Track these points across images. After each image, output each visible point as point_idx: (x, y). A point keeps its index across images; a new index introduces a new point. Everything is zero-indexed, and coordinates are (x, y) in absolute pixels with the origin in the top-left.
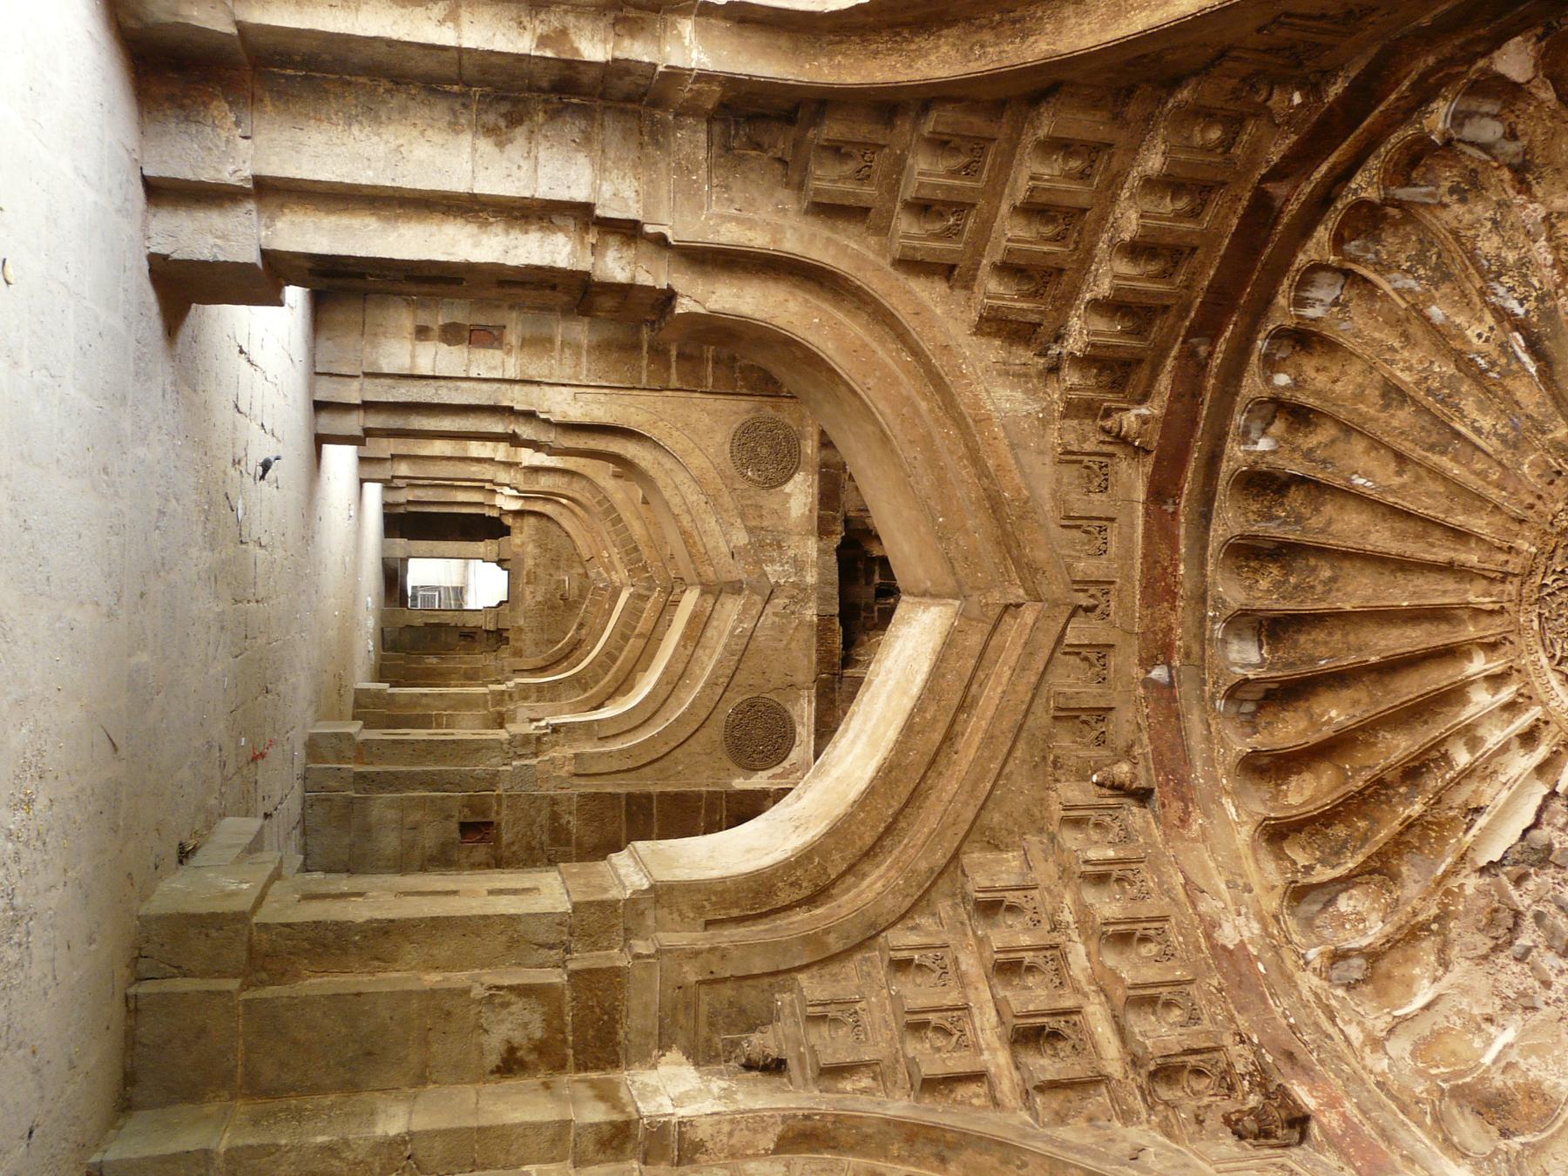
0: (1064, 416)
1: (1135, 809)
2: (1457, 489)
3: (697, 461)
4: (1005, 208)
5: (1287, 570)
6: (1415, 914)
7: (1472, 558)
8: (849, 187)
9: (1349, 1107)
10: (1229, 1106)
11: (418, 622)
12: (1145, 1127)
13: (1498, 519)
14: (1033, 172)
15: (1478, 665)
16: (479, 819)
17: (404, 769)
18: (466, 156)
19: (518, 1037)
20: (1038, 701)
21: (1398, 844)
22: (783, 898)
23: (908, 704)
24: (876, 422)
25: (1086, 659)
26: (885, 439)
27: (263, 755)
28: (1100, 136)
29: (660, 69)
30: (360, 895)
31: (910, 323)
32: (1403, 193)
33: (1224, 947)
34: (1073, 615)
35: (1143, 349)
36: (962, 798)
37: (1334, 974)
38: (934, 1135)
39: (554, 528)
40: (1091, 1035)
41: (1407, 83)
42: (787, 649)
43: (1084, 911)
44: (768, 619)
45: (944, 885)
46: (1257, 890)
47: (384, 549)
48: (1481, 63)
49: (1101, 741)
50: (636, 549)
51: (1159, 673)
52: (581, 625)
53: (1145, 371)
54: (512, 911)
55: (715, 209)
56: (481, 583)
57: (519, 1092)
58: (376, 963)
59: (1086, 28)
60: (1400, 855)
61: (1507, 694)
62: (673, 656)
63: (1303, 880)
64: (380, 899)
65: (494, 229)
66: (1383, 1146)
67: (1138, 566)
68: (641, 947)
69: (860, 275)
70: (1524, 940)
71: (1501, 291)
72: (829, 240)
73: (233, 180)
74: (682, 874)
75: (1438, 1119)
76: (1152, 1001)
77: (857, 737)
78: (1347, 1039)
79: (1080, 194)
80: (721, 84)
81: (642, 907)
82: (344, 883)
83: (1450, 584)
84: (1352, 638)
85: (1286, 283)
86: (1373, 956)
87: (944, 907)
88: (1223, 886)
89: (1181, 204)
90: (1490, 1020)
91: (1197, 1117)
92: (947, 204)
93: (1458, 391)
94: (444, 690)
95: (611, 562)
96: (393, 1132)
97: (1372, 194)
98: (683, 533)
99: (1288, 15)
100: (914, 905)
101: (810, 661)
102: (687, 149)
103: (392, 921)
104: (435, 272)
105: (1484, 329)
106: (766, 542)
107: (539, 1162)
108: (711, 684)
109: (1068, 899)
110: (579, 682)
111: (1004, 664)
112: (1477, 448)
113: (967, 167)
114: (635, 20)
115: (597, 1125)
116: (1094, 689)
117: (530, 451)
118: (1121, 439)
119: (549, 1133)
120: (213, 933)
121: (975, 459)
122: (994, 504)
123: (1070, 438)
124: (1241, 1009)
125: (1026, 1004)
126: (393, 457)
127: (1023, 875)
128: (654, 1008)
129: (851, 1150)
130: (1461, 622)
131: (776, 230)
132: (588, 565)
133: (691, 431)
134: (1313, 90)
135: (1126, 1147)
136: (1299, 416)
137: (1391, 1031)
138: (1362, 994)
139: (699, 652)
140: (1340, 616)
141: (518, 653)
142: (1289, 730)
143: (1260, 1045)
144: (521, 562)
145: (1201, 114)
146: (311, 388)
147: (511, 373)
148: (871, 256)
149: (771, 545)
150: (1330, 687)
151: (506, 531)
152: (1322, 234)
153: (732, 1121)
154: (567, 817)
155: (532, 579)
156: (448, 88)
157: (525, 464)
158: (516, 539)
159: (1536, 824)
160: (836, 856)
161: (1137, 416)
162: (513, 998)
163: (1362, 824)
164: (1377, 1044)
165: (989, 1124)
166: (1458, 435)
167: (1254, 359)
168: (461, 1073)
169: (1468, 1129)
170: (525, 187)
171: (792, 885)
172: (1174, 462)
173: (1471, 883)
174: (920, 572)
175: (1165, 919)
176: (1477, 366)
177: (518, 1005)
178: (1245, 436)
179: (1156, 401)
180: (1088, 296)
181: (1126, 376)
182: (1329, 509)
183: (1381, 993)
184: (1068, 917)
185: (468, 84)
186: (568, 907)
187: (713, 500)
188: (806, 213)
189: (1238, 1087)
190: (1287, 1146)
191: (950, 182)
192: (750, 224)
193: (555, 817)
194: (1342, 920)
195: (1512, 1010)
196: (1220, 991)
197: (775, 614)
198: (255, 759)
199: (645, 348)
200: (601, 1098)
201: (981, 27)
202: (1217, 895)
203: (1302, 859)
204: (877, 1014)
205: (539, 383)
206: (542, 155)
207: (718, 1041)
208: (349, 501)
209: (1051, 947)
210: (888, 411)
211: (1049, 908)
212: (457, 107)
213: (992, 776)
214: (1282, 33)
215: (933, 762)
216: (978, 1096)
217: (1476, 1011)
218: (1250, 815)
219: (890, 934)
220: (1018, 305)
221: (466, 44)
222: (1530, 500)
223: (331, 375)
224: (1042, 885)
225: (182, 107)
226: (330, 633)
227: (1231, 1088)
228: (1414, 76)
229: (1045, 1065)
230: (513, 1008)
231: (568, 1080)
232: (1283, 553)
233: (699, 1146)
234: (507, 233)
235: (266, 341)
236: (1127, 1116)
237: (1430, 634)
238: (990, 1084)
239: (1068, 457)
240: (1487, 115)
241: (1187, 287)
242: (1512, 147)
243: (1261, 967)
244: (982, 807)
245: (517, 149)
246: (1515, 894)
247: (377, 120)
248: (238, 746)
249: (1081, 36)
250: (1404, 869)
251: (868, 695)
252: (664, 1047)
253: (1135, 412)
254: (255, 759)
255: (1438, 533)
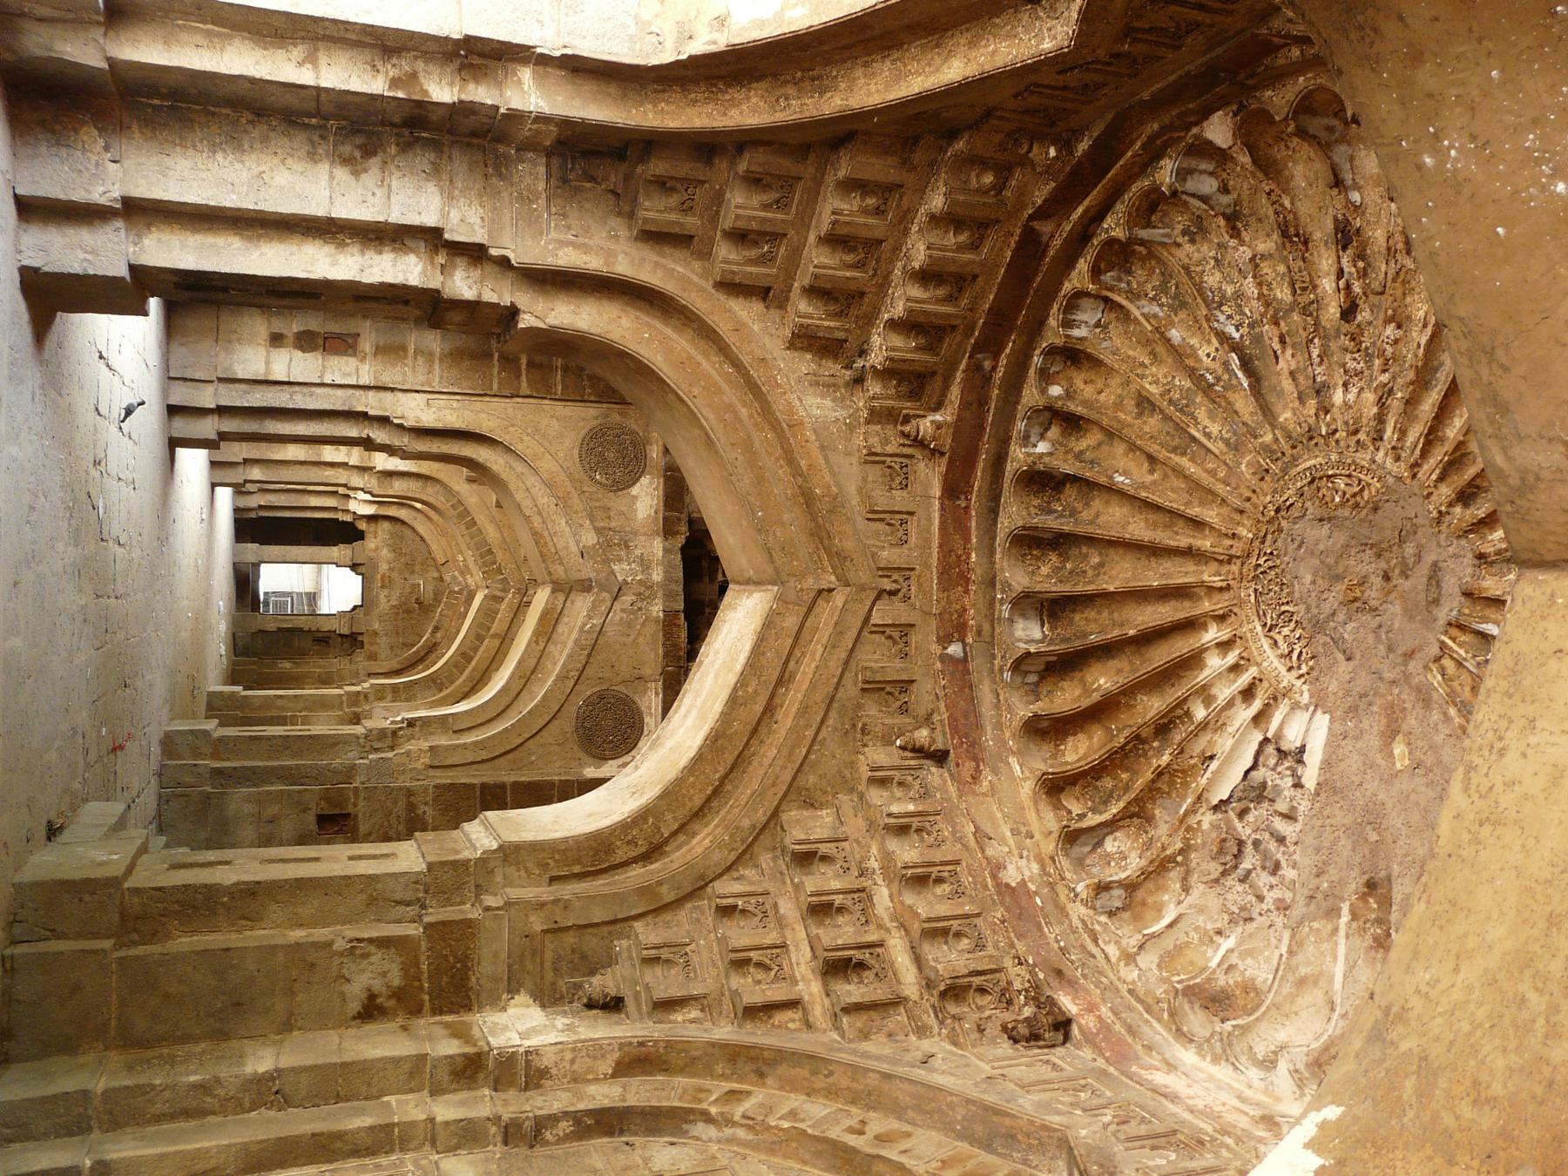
0: (868, 422)
1: (933, 769)
2: (1194, 485)
3: (547, 465)
4: (812, 238)
5: (1065, 557)
6: (1164, 848)
7: (1205, 543)
8: (673, 217)
9: (1104, 1011)
10: (1007, 1017)
11: (271, 627)
12: (937, 1039)
13: (1225, 511)
14: (834, 208)
15: (1212, 634)
16: (337, 811)
17: (261, 764)
18: (324, 183)
19: (378, 985)
20: (847, 674)
21: (1152, 791)
22: (621, 855)
23: (732, 679)
24: (702, 427)
25: (890, 637)
26: (709, 442)
27: (122, 748)
28: (891, 179)
29: (502, 110)
30: (227, 863)
31: (731, 338)
32: (1144, 234)
33: (1007, 885)
34: (878, 598)
35: (936, 364)
36: (780, 762)
37: (1098, 904)
38: (753, 1053)
39: (408, 532)
40: (892, 965)
41: (1139, 144)
42: (635, 643)
43: (887, 857)
44: (617, 615)
45: (766, 839)
46: (1037, 836)
47: (235, 553)
48: (1195, 130)
49: (904, 710)
50: (490, 552)
51: (955, 649)
52: (436, 629)
53: (937, 383)
54: (371, 872)
55: (553, 234)
56: (337, 589)
57: (379, 1034)
58: (243, 922)
59: (873, 88)
60: (1153, 800)
61: (1231, 658)
62: (525, 651)
63: (1075, 825)
64: (244, 866)
65: (350, 249)
66: (1130, 1040)
67: (935, 554)
68: (490, 901)
69: (685, 295)
70: (1246, 864)
71: (1222, 318)
72: (657, 263)
73: (103, 201)
74: (528, 836)
75: (1173, 1014)
76: (944, 932)
77: (688, 712)
78: (1107, 957)
79: (875, 226)
80: (557, 125)
81: (492, 865)
82: (211, 855)
83: (1190, 566)
84: (1116, 615)
85: (1056, 307)
86: (1131, 887)
87: (765, 860)
88: (1008, 834)
89: (962, 238)
90: (1219, 933)
91: (979, 1026)
92: (762, 234)
93: (1194, 402)
94: (299, 692)
95: (466, 566)
96: (261, 1069)
97: (1119, 233)
98: (535, 533)
99: (1037, 85)
100: (739, 858)
101: (657, 655)
102: (528, 180)
103: (258, 883)
104: (295, 287)
105: (1211, 349)
106: (614, 542)
107: (399, 1092)
108: (562, 678)
109: (874, 850)
110: (435, 682)
111: (818, 642)
112: (1209, 450)
113: (778, 202)
114: (479, 67)
115: (451, 1057)
116: (898, 663)
117: (384, 455)
118: (919, 443)
119: (407, 1066)
120: (87, 898)
121: (790, 459)
122: (807, 499)
123: (874, 440)
124: (1020, 936)
125: (835, 939)
126: (246, 461)
127: (836, 829)
128: (504, 955)
129: (681, 1071)
130: (1200, 598)
131: (610, 255)
132: (443, 569)
133: (541, 436)
134: (1066, 145)
135: (919, 1055)
136: (1073, 423)
137: (1141, 947)
138: (1121, 919)
139: (551, 647)
140: (1106, 596)
141: (373, 657)
142: (1066, 697)
143: (1035, 965)
144: (375, 567)
145: (974, 161)
146: (165, 393)
147: (365, 380)
148: (695, 278)
149: (619, 545)
150: (1099, 659)
151: (360, 536)
152: (1083, 265)
153: (574, 1050)
154: (423, 808)
155: (387, 583)
156: (307, 121)
157: (379, 468)
158: (370, 543)
159: (1254, 767)
160: (669, 816)
161: (932, 422)
162: (372, 949)
163: (1124, 776)
164: (1129, 958)
165: (802, 1042)
166: (1194, 439)
167: (1032, 372)
168: (325, 1019)
169: (1197, 1021)
170: (379, 212)
171: (628, 843)
172: (968, 463)
173: (1207, 819)
174: (744, 562)
175: (957, 862)
176: (1206, 380)
177: (377, 956)
178: (1026, 440)
179: (949, 409)
180: (886, 316)
181: (922, 387)
182: (1097, 504)
183: (1137, 918)
184: (874, 864)
185: (326, 118)
186: (421, 866)
187: (563, 502)
188: (636, 239)
189: (1015, 1001)
190: (1053, 1046)
191: (763, 214)
192: (585, 249)
193: (411, 807)
194: (1108, 858)
195: (1236, 923)
196: (1003, 922)
197: (623, 610)
198: (114, 750)
199: (496, 356)
200: (455, 1035)
201: (786, 82)
202: (1003, 842)
203: (1076, 808)
204: (705, 955)
205: (392, 390)
206: (395, 183)
207: (562, 985)
208: (201, 504)
209: (859, 891)
210: (711, 417)
211: (858, 856)
212: (316, 138)
213: (807, 742)
214: (1034, 100)
215: (755, 731)
216: (793, 1021)
217: (1209, 926)
218: (1032, 771)
219: (716, 884)
220: (826, 323)
221: (324, 85)
222: (1248, 494)
223: (185, 380)
224: (852, 837)
225: (53, 132)
226: (183, 634)
227: (1010, 1002)
228: (1144, 138)
229: (851, 991)
230: (373, 959)
231: (423, 1023)
232: (1060, 542)
233: (544, 1073)
234: (363, 254)
235: (123, 350)
236: (922, 1031)
237: (1176, 610)
238: (804, 1009)
239: (872, 458)
240: (1205, 172)
241: (971, 310)
242: (1225, 200)
243: (1038, 900)
244: (799, 770)
245: (371, 178)
246: (1239, 825)
247: (239, 148)
248: (99, 736)
249: (869, 94)
250: (1157, 812)
251: (698, 675)
252: (513, 990)
253: (930, 418)
254: (114, 750)
255: (1181, 523)
